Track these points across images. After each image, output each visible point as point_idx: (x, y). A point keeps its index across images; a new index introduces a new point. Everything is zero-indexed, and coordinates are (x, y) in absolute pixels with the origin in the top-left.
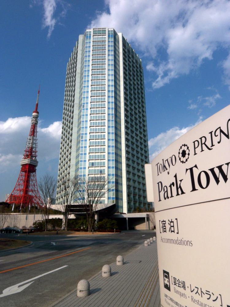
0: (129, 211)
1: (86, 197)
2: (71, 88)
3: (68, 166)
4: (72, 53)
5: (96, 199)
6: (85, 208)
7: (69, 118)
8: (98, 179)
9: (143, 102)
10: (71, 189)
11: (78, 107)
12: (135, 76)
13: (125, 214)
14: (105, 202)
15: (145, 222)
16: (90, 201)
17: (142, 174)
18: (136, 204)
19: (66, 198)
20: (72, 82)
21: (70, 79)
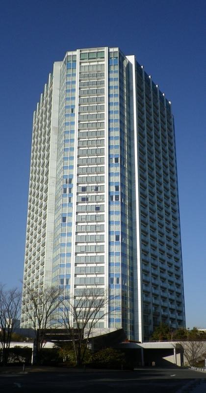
0: (145, 339)
1: (71, 318)
2: (38, 153)
3: (40, 272)
4: (35, 112)
5: (90, 321)
6: (69, 334)
7: (35, 207)
8: (93, 293)
9: (172, 173)
10: (45, 306)
11: (55, 182)
12: (165, 138)
13: (140, 343)
14: (103, 325)
15: (173, 354)
16: (78, 324)
17: (169, 284)
18: (157, 318)
19: (37, 320)
20: (40, 144)
21: (39, 131)
